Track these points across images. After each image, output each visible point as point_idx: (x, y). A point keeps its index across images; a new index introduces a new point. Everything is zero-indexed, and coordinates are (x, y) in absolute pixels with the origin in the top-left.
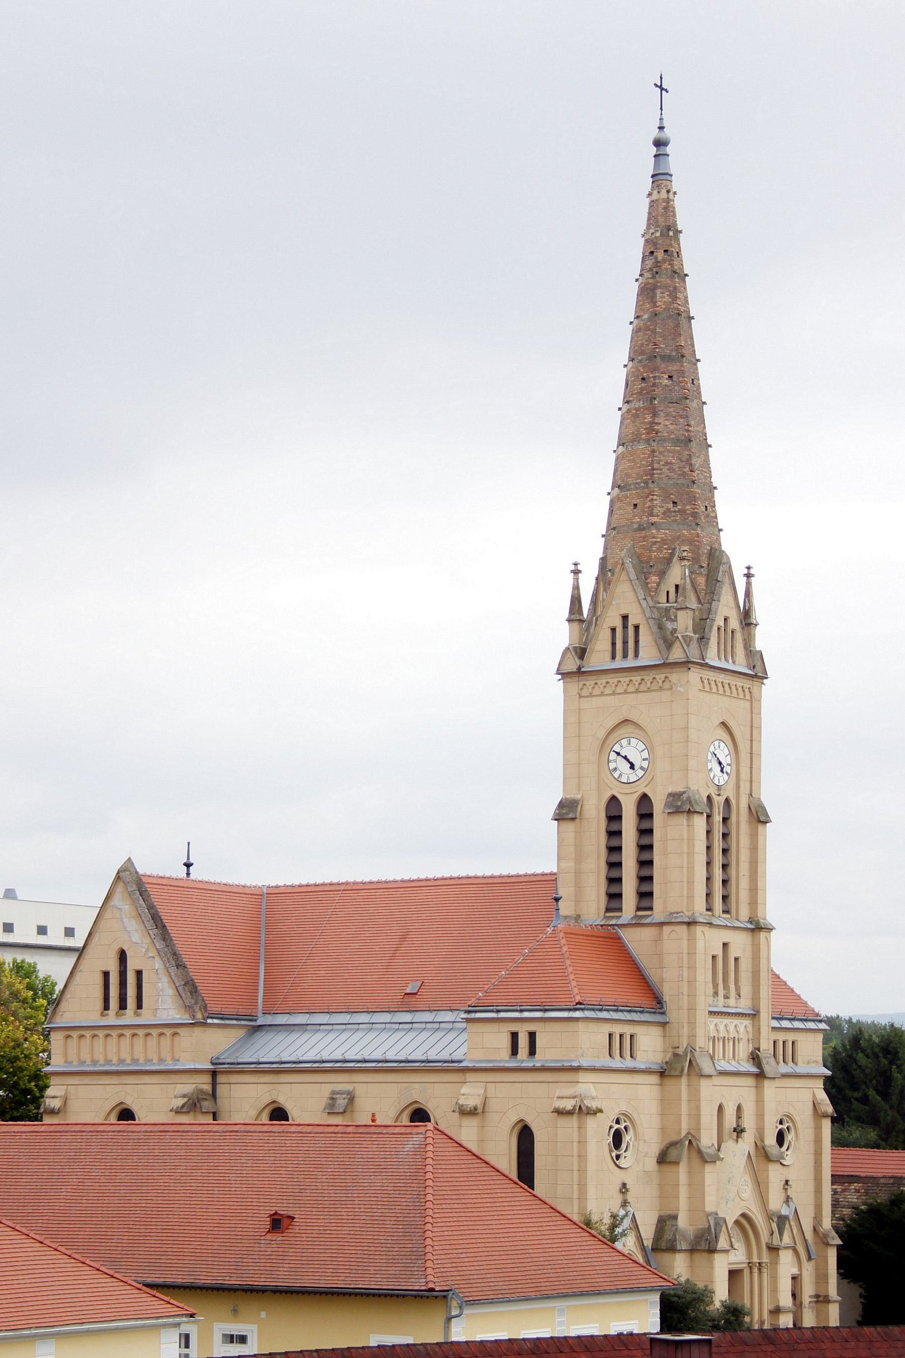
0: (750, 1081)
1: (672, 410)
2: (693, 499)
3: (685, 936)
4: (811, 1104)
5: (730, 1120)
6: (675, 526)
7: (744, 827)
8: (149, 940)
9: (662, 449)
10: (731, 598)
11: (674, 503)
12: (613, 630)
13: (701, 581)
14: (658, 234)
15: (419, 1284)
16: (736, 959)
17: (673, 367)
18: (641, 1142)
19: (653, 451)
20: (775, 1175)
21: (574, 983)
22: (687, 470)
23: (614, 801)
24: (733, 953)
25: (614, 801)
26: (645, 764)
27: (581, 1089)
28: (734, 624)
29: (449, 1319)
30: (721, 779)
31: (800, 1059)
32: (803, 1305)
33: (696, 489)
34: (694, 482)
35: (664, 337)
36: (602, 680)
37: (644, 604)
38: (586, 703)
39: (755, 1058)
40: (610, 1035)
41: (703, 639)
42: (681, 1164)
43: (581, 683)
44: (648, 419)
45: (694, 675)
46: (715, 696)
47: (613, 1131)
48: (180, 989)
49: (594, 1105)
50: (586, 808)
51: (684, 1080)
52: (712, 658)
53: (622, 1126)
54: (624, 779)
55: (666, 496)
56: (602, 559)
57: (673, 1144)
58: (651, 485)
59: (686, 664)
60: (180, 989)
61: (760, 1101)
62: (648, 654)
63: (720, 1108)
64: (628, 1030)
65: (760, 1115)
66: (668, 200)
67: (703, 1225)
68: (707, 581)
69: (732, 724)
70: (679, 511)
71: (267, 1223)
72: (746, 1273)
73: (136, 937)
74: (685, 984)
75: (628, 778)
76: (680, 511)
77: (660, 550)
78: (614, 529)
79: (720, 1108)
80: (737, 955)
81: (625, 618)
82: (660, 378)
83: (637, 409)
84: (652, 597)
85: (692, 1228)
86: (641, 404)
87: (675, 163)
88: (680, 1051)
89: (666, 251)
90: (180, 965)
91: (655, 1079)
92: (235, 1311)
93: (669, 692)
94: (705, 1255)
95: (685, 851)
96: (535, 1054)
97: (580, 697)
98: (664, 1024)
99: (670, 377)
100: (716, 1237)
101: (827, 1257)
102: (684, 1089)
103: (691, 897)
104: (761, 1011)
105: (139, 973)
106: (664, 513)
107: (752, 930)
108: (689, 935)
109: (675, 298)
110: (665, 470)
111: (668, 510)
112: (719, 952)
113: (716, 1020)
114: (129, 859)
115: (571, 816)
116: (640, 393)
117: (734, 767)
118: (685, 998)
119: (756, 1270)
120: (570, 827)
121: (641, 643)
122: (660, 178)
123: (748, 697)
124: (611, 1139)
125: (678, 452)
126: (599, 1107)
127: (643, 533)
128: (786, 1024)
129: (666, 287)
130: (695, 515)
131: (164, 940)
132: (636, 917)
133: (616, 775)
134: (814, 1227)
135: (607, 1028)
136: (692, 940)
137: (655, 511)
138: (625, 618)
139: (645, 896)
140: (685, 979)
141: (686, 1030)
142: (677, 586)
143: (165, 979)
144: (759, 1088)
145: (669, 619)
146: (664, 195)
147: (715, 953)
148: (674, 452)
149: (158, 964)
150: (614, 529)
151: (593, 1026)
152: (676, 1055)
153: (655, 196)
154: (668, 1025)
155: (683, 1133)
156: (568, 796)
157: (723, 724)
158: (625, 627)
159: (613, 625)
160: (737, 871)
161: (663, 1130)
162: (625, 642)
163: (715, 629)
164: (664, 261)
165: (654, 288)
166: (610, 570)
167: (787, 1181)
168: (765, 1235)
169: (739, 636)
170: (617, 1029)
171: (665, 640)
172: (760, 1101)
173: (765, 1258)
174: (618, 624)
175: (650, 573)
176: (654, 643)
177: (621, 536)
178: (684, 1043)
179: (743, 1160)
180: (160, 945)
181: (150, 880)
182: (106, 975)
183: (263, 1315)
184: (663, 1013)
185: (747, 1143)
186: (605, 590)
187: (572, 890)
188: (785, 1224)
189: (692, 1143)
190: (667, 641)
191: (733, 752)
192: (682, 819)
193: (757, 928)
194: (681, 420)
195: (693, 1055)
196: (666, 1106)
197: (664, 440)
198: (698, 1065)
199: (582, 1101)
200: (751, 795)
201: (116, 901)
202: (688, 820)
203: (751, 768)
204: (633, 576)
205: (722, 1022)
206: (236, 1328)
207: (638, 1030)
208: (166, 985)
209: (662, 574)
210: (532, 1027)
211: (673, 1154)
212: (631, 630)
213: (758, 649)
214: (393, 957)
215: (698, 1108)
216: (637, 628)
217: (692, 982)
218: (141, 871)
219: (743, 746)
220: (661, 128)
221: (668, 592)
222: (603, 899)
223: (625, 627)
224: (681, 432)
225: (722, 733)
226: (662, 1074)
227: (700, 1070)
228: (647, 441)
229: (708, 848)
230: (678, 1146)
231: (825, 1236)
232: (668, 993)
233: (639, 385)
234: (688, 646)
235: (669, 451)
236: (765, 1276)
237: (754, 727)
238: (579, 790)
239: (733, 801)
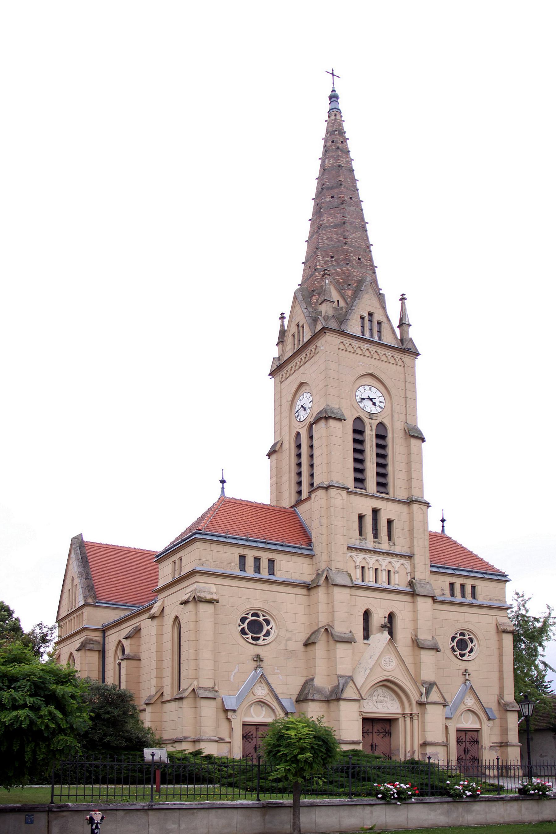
1: (332, 212)
9: (324, 232)
11: (332, 257)
32: (484, 747)
37: (305, 311)
43: (281, 375)
67: (335, 683)
70: (335, 260)
72: (401, 721)
82: (325, 198)
85: (330, 687)
87: (342, 105)
88: (320, 572)
94: (335, 703)
99: (332, 197)
100: (342, 690)
104: (415, 553)
106: (324, 263)
110: (326, 242)
111: (328, 261)
113: (353, 554)
119: (408, 719)
125: (335, 231)
134: (498, 701)
147: (362, 512)
152: (318, 575)
154: (314, 557)
160: (393, 467)
164: (331, 146)
168: (415, 695)
173: (416, 709)
184: (311, 550)
195: (328, 573)
197: (327, 227)
202: (326, 424)
212: (301, 329)
216: (303, 327)
224: (338, 221)
231: (506, 705)
235: (330, 232)
236: (416, 722)
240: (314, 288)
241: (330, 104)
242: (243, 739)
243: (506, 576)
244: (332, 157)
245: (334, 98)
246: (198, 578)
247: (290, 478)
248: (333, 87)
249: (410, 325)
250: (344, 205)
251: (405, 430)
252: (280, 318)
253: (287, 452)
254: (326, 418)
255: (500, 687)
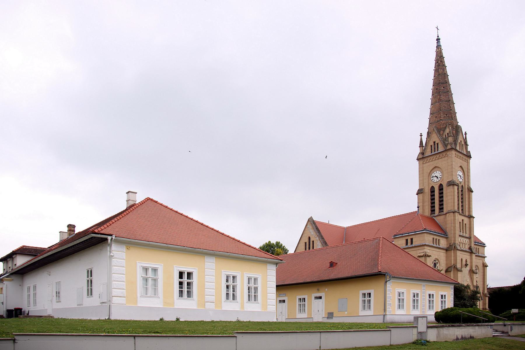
0: (469, 254)
2: (451, 113)
3: (453, 216)
4: (482, 264)
5: (464, 263)
6: (447, 120)
7: (467, 193)
8: (315, 233)
9: (442, 103)
10: (462, 136)
11: (446, 115)
12: (431, 146)
13: (454, 132)
14: (439, 58)
15: (375, 271)
16: (465, 224)
17: (444, 85)
18: (441, 266)
19: (440, 104)
20: (475, 276)
21: (423, 225)
22: (449, 107)
23: (433, 187)
24: (465, 222)
25: (433, 187)
26: (441, 177)
27: (425, 250)
28: (463, 143)
29: (386, 282)
30: (461, 180)
31: (480, 253)
33: (451, 111)
34: (451, 110)
35: (442, 79)
36: (429, 159)
37: (439, 137)
38: (424, 165)
39: (470, 248)
40: (433, 239)
41: (456, 144)
42: (452, 272)
43: (423, 161)
44: (439, 97)
45: (453, 152)
46: (459, 159)
47: (434, 263)
48: (322, 243)
49: (429, 254)
50: (425, 190)
51: (452, 251)
52: (458, 148)
53: (436, 262)
54: (435, 181)
55: (444, 114)
56: (428, 132)
57: (450, 267)
58: (440, 111)
59: (452, 149)
60: (322, 243)
61: (471, 259)
62: (441, 149)
63: (462, 259)
64: (438, 238)
65: (471, 262)
66: (441, 51)
68: (456, 132)
69: (463, 167)
71: (329, 265)
73: (312, 233)
74: (453, 228)
75: (436, 181)
76: (449, 117)
77: (443, 125)
78: (431, 123)
79: (462, 259)
80: (466, 223)
81: (434, 142)
82: (441, 88)
83: (435, 96)
84: (441, 136)
86: (436, 94)
87: (442, 43)
88: (451, 244)
89: (441, 61)
90: (323, 238)
91: (444, 251)
92: (318, 290)
93: (447, 157)
95: (452, 195)
96: (412, 244)
97: (423, 164)
98: (447, 238)
99: (444, 87)
101: (486, 299)
102: (452, 253)
103: (454, 206)
105: (313, 241)
107: (469, 218)
108: (454, 215)
109: (444, 70)
110: (444, 108)
111: (445, 116)
112: (461, 221)
113: (460, 238)
114: (311, 217)
115: (421, 192)
116: (436, 92)
117: (464, 177)
118: (453, 231)
120: (421, 195)
121: (439, 147)
122: (439, 47)
123: (467, 161)
124: (433, 265)
126: (430, 255)
127: (438, 123)
128: (477, 244)
129: (442, 68)
130: (452, 117)
131: (319, 233)
132: (439, 214)
133: (433, 181)
135: (432, 236)
136: (454, 216)
137: (441, 117)
138: (434, 142)
139: (441, 209)
140: (453, 226)
141: (453, 239)
142: (448, 133)
143: (319, 242)
144: (471, 256)
145: (446, 141)
146: (440, 50)
147: (460, 221)
148: (446, 103)
149: (317, 238)
150: (431, 123)
151: (429, 235)
152: (450, 245)
153: (438, 50)
155: (452, 265)
156: (420, 188)
157: (461, 166)
158: (434, 145)
159: (431, 145)
161: (447, 264)
162: (435, 148)
163: (458, 143)
164: (440, 63)
165: (438, 70)
166: (430, 133)
167: (477, 281)
169: (464, 146)
170: (435, 237)
171: (445, 145)
172: (471, 259)
174: (433, 144)
175: (440, 131)
176: (442, 146)
177: (433, 124)
178: (453, 242)
179: (468, 272)
180: (318, 234)
181: (317, 222)
182: (306, 243)
183: (326, 290)
185: (468, 268)
186: (429, 138)
187: (422, 210)
188: (478, 288)
189: (455, 267)
190: (445, 145)
191: (463, 174)
192: (452, 187)
193: (471, 217)
194: (447, 96)
195: (455, 245)
196: (448, 258)
197: (443, 101)
198: (456, 247)
199: (426, 253)
200: (468, 185)
201: (308, 226)
202: (453, 187)
203: (468, 179)
204: (436, 131)
205: (462, 239)
206: (318, 295)
207: (441, 239)
208: (319, 243)
209: (444, 131)
210: (411, 237)
211: (450, 269)
212: (436, 145)
213: (468, 151)
214: (376, 234)
215: (456, 258)
216: (438, 144)
217: (455, 227)
218: (314, 220)
219: (466, 173)
220: (438, 36)
221: (446, 135)
222: (430, 211)
223: (434, 145)
225: (460, 169)
226: (447, 250)
227: (457, 248)
228: (439, 102)
229: (458, 196)
230: (451, 268)
231: (486, 294)
232: (448, 230)
233: (436, 91)
234: (452, 145)
235: (444, 103)
237: (468, 169)
238: (423, 186)
239: (464, 186)
240: (441, 127)
241: (437, 43)
242: (226, 295)
243: (485, 244)
244: (442, 68)
245: (438, 40)
246: (426, 247)
247: (429, 204)
248: (438, 35)
249: (468, 145)
250: (448, 92)
251: (468, 188)
252: (420, 135)
253: (427, 194)
254: (453, 185)
255: (483, 288)
